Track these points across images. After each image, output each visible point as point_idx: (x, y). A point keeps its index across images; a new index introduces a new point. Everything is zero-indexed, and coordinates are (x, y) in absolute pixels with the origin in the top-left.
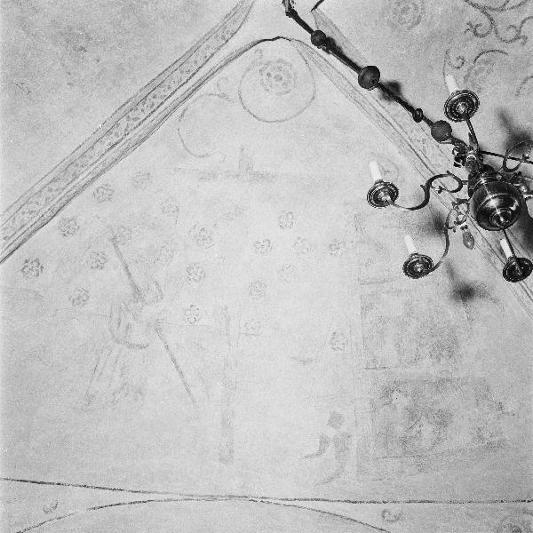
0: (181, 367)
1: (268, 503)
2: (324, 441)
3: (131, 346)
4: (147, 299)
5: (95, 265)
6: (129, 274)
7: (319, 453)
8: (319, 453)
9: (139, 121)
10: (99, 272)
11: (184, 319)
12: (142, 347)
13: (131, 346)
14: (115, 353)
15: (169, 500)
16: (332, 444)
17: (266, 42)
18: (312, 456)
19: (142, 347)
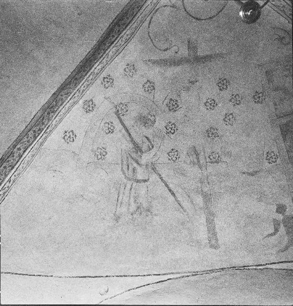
0: (170, 194)
1: (249, 269)
2: (276, 224)
3: (138, 181)
4: (143, 149)
5: (107, 131)
6: (130, 135)
7: (276, 230)
8: (276, 230)
9: (126, 25)
10: (110, 135)
11: (169, 159)
12: (145, 181)
13: (138, 181)
14: (129, 186)
15: (183, 277)
16: (282, 225)
17: (93, 276)
18: (271, 235)
19: (145, 181)
